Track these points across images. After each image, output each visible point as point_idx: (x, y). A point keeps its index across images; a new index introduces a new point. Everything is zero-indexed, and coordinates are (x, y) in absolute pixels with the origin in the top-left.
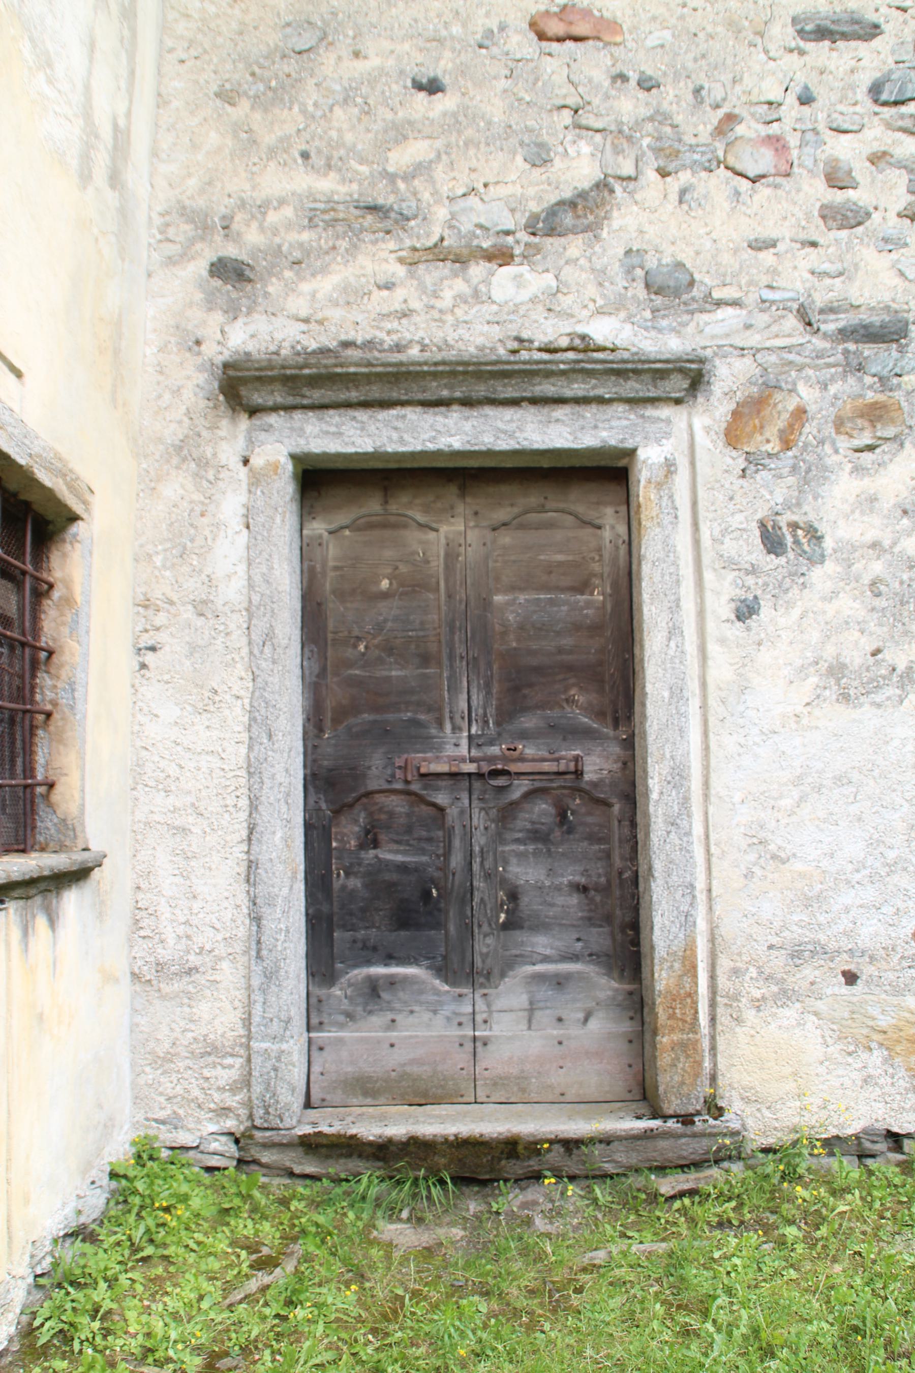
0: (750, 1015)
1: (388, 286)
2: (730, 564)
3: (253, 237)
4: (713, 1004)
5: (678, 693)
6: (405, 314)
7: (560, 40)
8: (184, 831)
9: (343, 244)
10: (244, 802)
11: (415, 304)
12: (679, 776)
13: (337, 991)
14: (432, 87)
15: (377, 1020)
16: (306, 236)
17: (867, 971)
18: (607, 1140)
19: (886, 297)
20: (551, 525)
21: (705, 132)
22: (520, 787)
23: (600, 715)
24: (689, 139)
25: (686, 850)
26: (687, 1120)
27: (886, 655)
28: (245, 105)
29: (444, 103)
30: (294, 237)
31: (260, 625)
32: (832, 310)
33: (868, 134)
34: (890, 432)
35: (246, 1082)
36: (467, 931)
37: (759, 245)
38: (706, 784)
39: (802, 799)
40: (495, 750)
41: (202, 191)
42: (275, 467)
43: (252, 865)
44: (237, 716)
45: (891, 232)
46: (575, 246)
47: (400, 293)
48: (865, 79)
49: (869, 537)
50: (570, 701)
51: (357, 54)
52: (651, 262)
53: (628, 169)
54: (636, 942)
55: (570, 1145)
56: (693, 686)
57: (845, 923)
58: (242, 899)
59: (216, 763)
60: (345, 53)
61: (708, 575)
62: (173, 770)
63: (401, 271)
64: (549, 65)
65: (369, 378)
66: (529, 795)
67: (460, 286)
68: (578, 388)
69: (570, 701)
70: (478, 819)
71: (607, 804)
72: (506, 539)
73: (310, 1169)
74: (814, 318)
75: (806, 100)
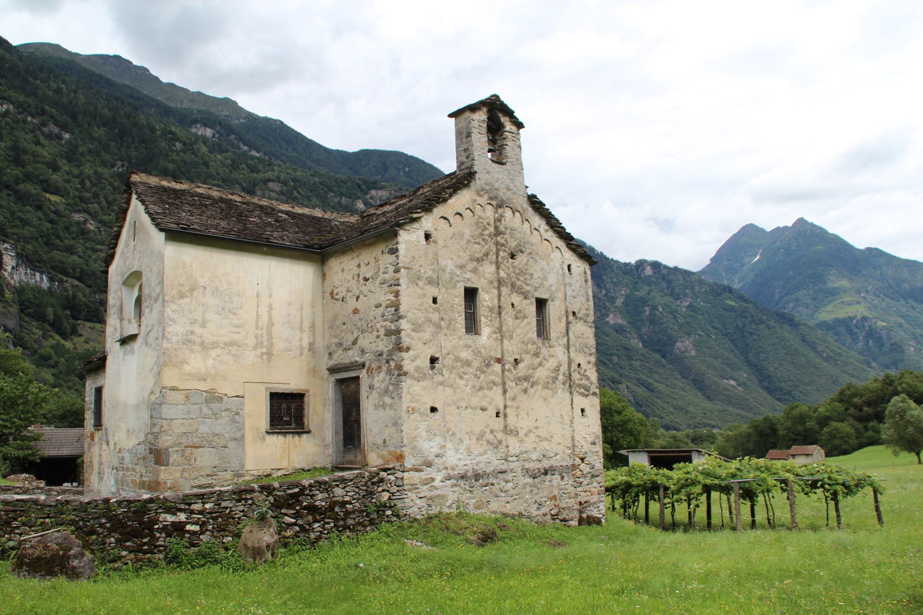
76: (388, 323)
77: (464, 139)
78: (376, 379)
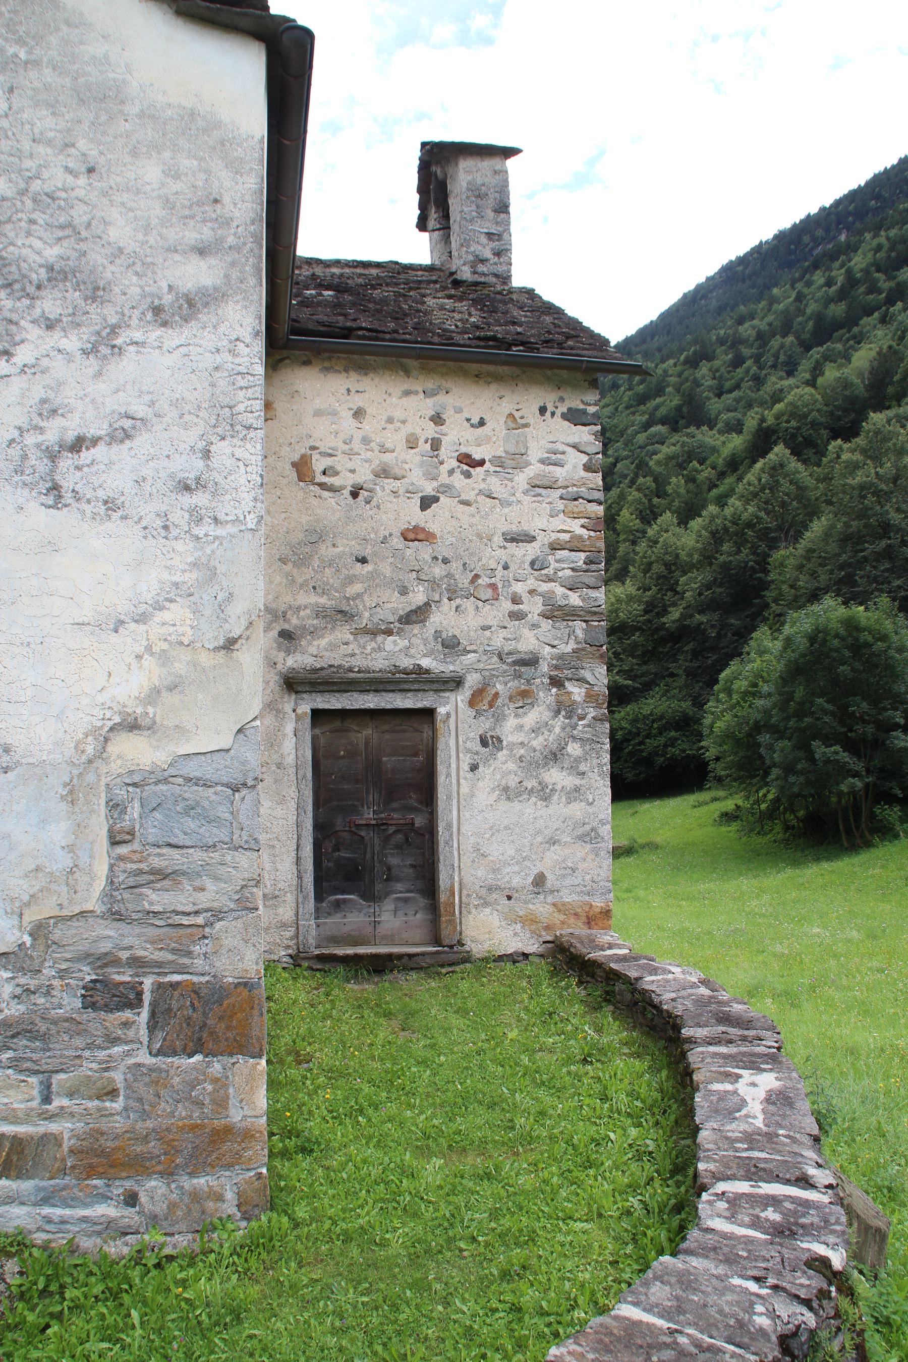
0: (473, 910)
1: (346, 644)
2: (469, 751)
3: (295, 621)
4: (460, 907)
5: (449, 797)
6: (353, 655)
7: (413, 541)
8: (274, 847)
9: (330, 626)
10: (295, 836)
11: (357, 652)
12: (449, 826)
13: (324, 904)
14: (363, 561)
15: (339, 915)
16: (315, 622)
17: (515, 895)
18: (423, 954)
19: (531, 648)
20: (404, 731)
21: (466, 582)
22: (392, 829)
23: (421, 802)
24: (460, 586)
25: (451, 853)
26: (451, 947)
27: (524, 783)
28: (290, 565)
29: (368, 568)
30: (310, 622)
31: (301, 772)
32: (511, 654)
33: (529, 582)
34: (529, 701)
35: (297, 936)
36: (372, 882)
37: (485, 628)
38: (459, 829)
39: (493, 834)
40: (383, 815)
41: (274, 601)
42: (306, 713)
43: (298, 859)
44: (293, 805)
45: (535, 622)
46: (416, 629)
47: (351, 646)
48: (529, 559)
49: (520, 741)
50: (410, 797)
51: (334, 545)
52: (444, 635)
53: (437, 598)
54: (434, 885)
55: (411, 956)
56: (455, 794)
57: (507, 878)
58: (295, 871)
59: (285, 822)
60: (329, 544)
61: (461, 755)
62: (269, 825)
63: (351, 637)
64: (408, 552)
65: (341, 683)
66: (395, 832)
67: (373, 644)
68: (416, 686)
69: (410, 797)
70: (376, 841)
71: (423, 835)
72: (387, 736)
73: (319, 967)
74: (504, 657)
75: (506, 567)
76: (560, 591)
77: (490, 214)
78: (511, 722)
